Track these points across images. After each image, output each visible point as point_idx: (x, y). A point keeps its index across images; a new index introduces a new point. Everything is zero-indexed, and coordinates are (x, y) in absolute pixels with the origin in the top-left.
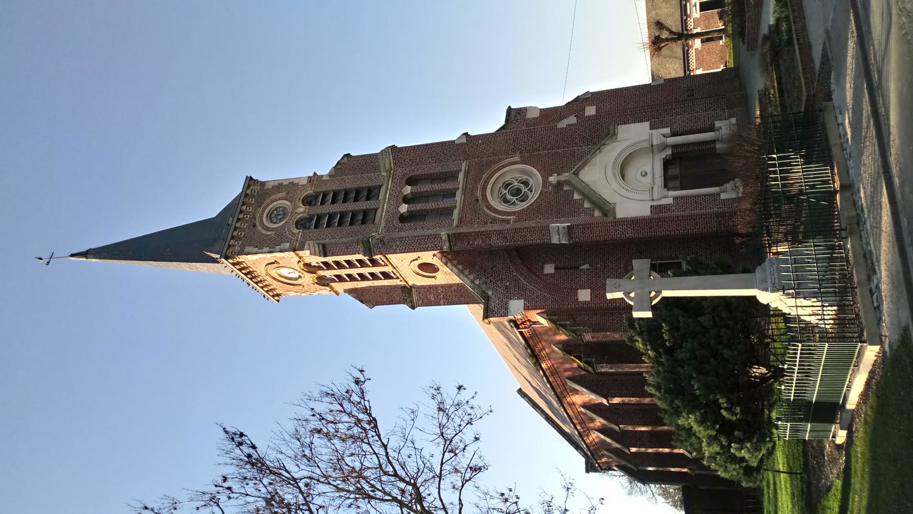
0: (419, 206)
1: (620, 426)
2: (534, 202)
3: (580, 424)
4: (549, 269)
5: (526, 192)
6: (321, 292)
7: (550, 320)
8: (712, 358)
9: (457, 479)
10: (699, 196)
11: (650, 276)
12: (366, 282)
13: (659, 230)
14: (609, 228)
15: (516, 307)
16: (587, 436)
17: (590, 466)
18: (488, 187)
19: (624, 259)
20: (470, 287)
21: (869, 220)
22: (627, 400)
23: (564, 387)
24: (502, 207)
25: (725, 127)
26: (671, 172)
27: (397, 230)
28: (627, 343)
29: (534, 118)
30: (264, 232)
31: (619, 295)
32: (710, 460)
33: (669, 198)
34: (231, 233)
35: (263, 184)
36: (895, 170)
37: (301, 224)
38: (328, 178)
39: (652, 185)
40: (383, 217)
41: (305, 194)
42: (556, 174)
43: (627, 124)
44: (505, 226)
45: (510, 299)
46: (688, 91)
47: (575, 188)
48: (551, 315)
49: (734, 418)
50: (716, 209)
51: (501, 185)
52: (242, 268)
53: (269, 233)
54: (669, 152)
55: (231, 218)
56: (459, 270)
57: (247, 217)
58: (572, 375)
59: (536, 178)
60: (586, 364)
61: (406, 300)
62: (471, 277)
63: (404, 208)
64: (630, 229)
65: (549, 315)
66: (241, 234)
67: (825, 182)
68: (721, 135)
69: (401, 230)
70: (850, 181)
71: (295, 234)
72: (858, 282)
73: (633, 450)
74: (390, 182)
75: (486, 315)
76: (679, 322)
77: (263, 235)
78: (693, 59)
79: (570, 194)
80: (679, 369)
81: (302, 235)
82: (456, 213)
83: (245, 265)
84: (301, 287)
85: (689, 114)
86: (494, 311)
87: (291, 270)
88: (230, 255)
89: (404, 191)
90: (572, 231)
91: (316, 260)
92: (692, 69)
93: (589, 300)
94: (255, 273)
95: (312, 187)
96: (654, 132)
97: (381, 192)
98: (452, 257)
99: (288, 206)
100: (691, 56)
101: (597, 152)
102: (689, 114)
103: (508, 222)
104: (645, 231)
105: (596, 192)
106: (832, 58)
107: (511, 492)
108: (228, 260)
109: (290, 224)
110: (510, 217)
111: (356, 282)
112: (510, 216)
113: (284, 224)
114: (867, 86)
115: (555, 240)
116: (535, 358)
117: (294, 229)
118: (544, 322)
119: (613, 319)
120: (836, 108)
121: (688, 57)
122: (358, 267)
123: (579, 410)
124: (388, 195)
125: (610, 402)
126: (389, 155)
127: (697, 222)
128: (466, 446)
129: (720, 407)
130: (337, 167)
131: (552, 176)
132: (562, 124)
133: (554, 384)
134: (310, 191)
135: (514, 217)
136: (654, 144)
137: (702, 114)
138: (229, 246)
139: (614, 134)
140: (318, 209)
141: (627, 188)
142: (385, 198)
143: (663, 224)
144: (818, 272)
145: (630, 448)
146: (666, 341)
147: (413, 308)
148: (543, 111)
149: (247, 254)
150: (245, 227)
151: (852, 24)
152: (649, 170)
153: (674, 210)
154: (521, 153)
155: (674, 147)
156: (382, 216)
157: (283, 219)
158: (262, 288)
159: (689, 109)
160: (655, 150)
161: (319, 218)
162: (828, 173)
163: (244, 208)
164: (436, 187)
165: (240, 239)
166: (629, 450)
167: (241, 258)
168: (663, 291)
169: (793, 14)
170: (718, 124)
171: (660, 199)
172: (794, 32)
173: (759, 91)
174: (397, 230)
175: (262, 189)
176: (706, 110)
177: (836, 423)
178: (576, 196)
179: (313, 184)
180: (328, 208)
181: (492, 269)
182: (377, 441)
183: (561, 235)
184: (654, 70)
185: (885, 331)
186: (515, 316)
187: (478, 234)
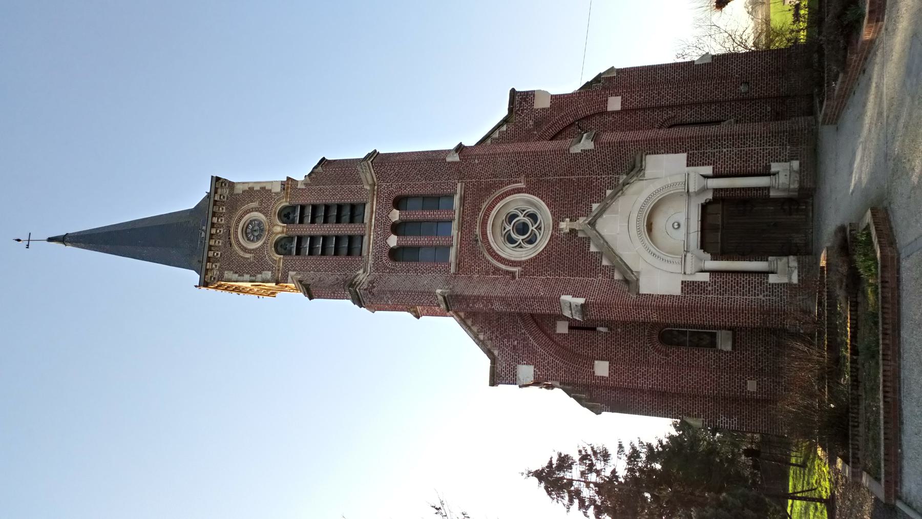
0: (410, 240)
2: (543, 251)
27: (388, 271)
30: (242, 253)
34: (205, 254)
38: (303, 187)
40: (371, 250)
41: (280, 207)
42: (568, 220)
43: (658, 153)
45: (518, 364)
50: (761, 297)
53: (247, 256)
54: (710, 196)
59: (545, 214)
63: (393, 241)
68: (777, 185)
71: (276, 261)
74: (375, 203)
77: (239, 256)
81: (283, 262)
82: (453, 252)
85: (739, 147)
86: (501, 376)
88: (209, 281)
97: (366, 213)
101: (619, 194)
109: (269, 245)
113: (262, 246)
119: (634, 397)
124: (373, 220)
126: (370, 169)
134: (285, 203)
135: (520, 268)
136: (690, 191)
137: (755, 150)
138: (207, 270)
139: (641, 169)
147: (418, 317)
148: (555, 98)
152: (683, 222)
153: (710, 291)
154: (527, 176)
155: (715, 190)
156: (369, 249)
157: (258, 238)
159: (739, 142)
163: (215, 220)
165: (217, 260)
170: (775, 167)
171: (694, 274)
174: (388, 271)
175: (231, 194)
176: (761, 144)
179: (287, 193)
180: (307, 229)
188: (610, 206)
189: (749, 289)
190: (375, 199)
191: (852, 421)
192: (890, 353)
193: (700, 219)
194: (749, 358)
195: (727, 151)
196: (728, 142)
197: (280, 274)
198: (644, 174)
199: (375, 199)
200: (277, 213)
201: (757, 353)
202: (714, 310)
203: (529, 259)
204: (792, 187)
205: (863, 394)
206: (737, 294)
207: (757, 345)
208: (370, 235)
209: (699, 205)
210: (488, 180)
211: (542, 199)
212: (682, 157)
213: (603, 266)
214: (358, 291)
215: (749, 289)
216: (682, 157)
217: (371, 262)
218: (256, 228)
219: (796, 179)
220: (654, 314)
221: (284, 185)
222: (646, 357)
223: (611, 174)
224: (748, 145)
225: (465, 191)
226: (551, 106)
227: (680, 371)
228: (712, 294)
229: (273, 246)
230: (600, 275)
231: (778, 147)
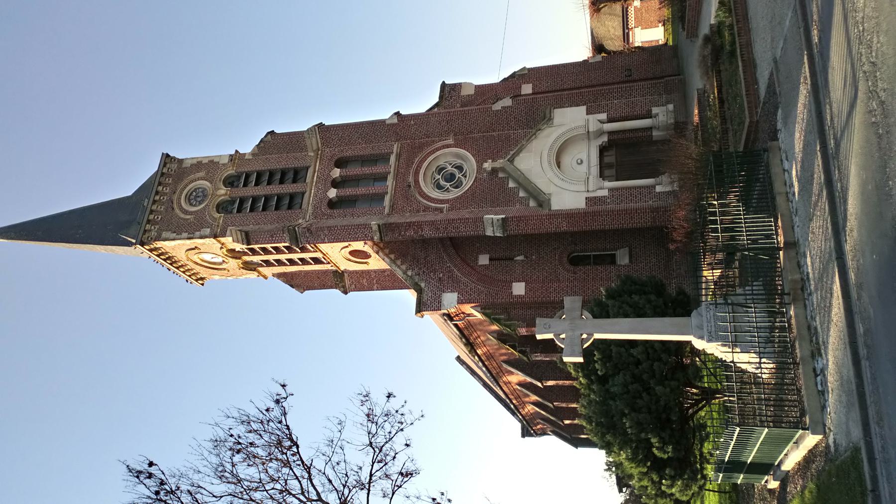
0: (348, 191)
1: (554, 403)
2: (468, 190)
3: (516, 399)
4: (484, 260)
5: (461, 178)
6: (248, 276)
7: (484, 314)
8: (645, 393)
9: (387, 485)
10: (635, 188)
11: (582, 315)
12: (296, 266)
13: (593, 224)
14: (544, 221)
15: (450, 299)
16: (523, 408)
17: (525, 431)
18: (421, 171)
19: (559, 251)
20: (402, 278)
21: (815, 295)
22: (561, 382)
23: (500, 369)
24: (435, 194)
25: (663, 114)
26: (607, 160)
28: (558, 365)
30: (182, 216)
31: (550, 336)
32: (640, 489)
33: (603, 189)
35: (181, 161)
36: (850, 263)
37: (222, 207)
38: (251, 157)
39: (588, 176)
40: (311, 202)
42: (490, 161)
43: (563, 107)
44: (437, 214)
45: (443, 292)
46: (626, 71)
47: (510, 176)
48: (485, 309)
49: (666, 456)
50: (651, 202)
51: (434, 169)
52: (160, 253)
53: (188, 217)
54: (605, 139)
55: (147, 200)
56: (391, 259)
57: (164, 198)
58: (508, 359)
59: (470, 163)
60: (520, 353)
61: (338, 284)
62: (404, 267)
63: (332, 193)
64: (565, 223)
65: (484, 309)
66: (158, 218)
67: (768, 237)
69: (330, 216)
70: (795, 238)
71: (216, 219)
72: (801, 358)
73: (567, 422)
74: (318, 164)
75: (421, 308)
76: (611, 350)
77: (180, 218)
78: (632, 17)
79: (505, 181)
80: (611, 402)
81: (223, 220)
82: (387, 199)
83: (163, 251)
84: (226, 272)
85: (626, 99)
86: (427, 304)
87: (214, 256)
88: (146, 241)
89: (333, 175)
90: (506, 224)
91: (239, 247)
92: (630, 28)
93: (523, 293)
94: (175, 258)
95: (233, 166)
96: (591, 117)
98: (384, 246)
99: (208, 187)
100: (630, 14)
101: (532, 138)
103: (441, 210)
104: (580, 225)
106: (780, 93)
107: (443, 496)
108: (144, 246)
109: (211, 207)
110: (443, 206)
111: (284, 267)
112: (443, 204)
113: (204, 208)
114: (820, 148)
115: (489, 233)
116: (471, 346)
117: (214, 214)
118: (479, 316)
119: (547, 313)
120: (782, 151)
121: (627, 21)
122: (286, 253)
123: (515, 387)
124: (315, 178)
125: (544, 384)
126: (316, 134)
127: (632, 216)
128: (397, 454)
129: (651, 446)
130: (261, 146)
131: (486, 162)
132: (498, 106)
133: (490, 367)
134: (231, 171)
135: (447, 205)
136: (590, 131)
137: (639, 100)
138: (145, 231)
139: (550, 119)
140: (241, 192)
141: (563, 177)
142: (313, 182)
143: (597, 218)
144: (759, 343)
145: (564, 421)
146: (598, 370)
147: (346, 293)
148: (479, 88)
149: (165, 240)
150: (162, 209)
151: (805, 67)
152: (585, 158)
153: (609, 203)
154: (455, 135)
155: (610, 133)
158: (184, 272)
160: (592, 136)
161: (242, 201)
162: (771, 226)
163: (160, 188)
164: (367, 170)
165: (157, 223)
166: (563, 423)
167: (159, 244)
168: (594, 334)
169: (737, 25)
170: (655, 110)
171: (596, 190)
172: (738, 45)
173: (698, 90)
174: (326, 217)
175: (179, 168)
176: (643, 94)
177: (771, 475)
178: (511, 184)
179: (234, 163)
180: (252, 190)
181: (425, 259)
182: (299, 465)
183: (495, 228)
184: (593, 27)
185: (828, 422)
186: (448, 309)
187: (410, 225)
188: (525, 147)
189: (641, 198)
190: (318, 162)
191: (724, 145)
192: (743, 32)
193: (598, 156)
194: (644, 268)
195: (618, 102)
196: (618, 94)
197: (219, 230)
198: (553, 122)
199: (318, 162)
200: (222, 180)
201: (650, 264)
202: (613, 213)
203: (456, 197)
204: (669, 122)
205: (731, 127)
206: (631, 202)
207: (650, 257)
208: (312, 189)
209: (597, 146)
210: (421, 140)
211: (468, 151)
212: (583, 109)
213: (520, 197)
214: (297, 229)
215: (641, 198)
216: (583, 109)
217: (310, 211)
218: (200, 194)
219: (672, 116)
220: (564, 223)
221: (232, 156)
222: (557, 277)
223: (525, 129)
224: (633, 96)
225: (400, 150)
226: (475, 93)
227: (586, 283)
228: (611, 204)
229: (215, 206)
230: (518, 204)
231: (656, 97)
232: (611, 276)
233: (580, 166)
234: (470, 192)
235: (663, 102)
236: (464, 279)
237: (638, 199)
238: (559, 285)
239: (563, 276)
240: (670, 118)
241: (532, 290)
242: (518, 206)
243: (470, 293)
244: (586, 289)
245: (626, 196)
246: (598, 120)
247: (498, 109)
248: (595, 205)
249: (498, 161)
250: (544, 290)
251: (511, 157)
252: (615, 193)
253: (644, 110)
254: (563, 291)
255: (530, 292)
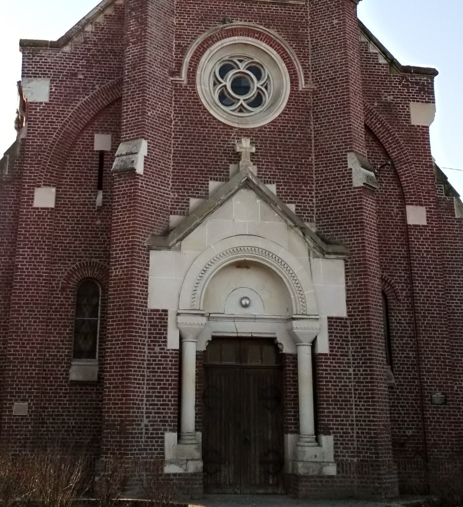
2: (210, 115)
5: (238, 102)
29: (409, 115)
42: (254, 150)
43: (346, 276)
45: (51, 80)
50: (146, 421)
51: (257, 61)
54: (287, 349)
64: (121, 273)
68: (302, 444)
85: (355, 390)
86: (34, 56)
101: (289, 221)
102: (355, 390)
105: (208, 219)
131: (251, 143)
135: (185, 82)
136: (294, 322)
137: (351, 413)
139: (324, 253)
148: (424, 132)
152: (249, 311)
154: (314, 93)
155: (295, 358)
159: (362, 390)
170: (327, 441)
171: (178, 328)
193: (255, 335)
194: (60, 404)
195: (350, 374)
196: (362, 375)
198: (318, 257)
202: (126, 355)
204: (300, 465)
206: (150, 388)
207: (78, 415)
209: (275, 334)
210: (309, 37)
211: (283, 113)
212: (341, 311)
213: (188, 200)
215: (157, 405)
216: (341, 311)
219: (311, 470)
222: (60, 260)
223: (318, 210)
224: (358, 403)
226: (413, 126)
227: (41, 308)
228: (149, 353)
230: (176, 196)
231: (355, 446)
232: (52, 348)
233: (238, 300)
234: (205, 118)
235: (344, 456)
236: (70, 111)
237: (153, 400)
238: (43, 262)
239: (60, 270)
240: (308, 468)
241: (39, 218)
242: (172, 196)
243: (45, 122)
244: (32, 307)
245: (162, 380)
246: (316, 337)
247: (348, 163)
248: (151, 326)
249: (252, 163)
250: (38, 238)
251: (254, 184)
252: (171, 361)
253: (328, 420)
254: (31, 269)
255: (36, 215)
